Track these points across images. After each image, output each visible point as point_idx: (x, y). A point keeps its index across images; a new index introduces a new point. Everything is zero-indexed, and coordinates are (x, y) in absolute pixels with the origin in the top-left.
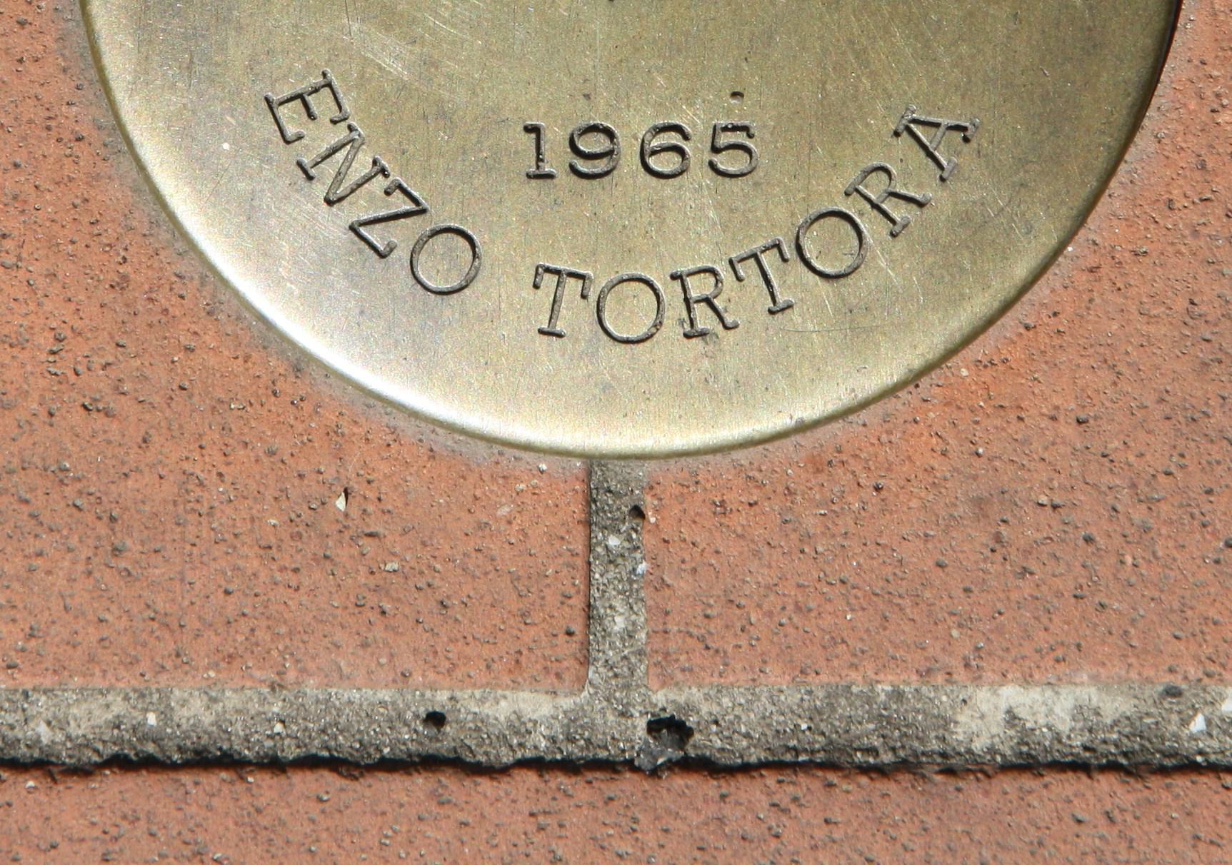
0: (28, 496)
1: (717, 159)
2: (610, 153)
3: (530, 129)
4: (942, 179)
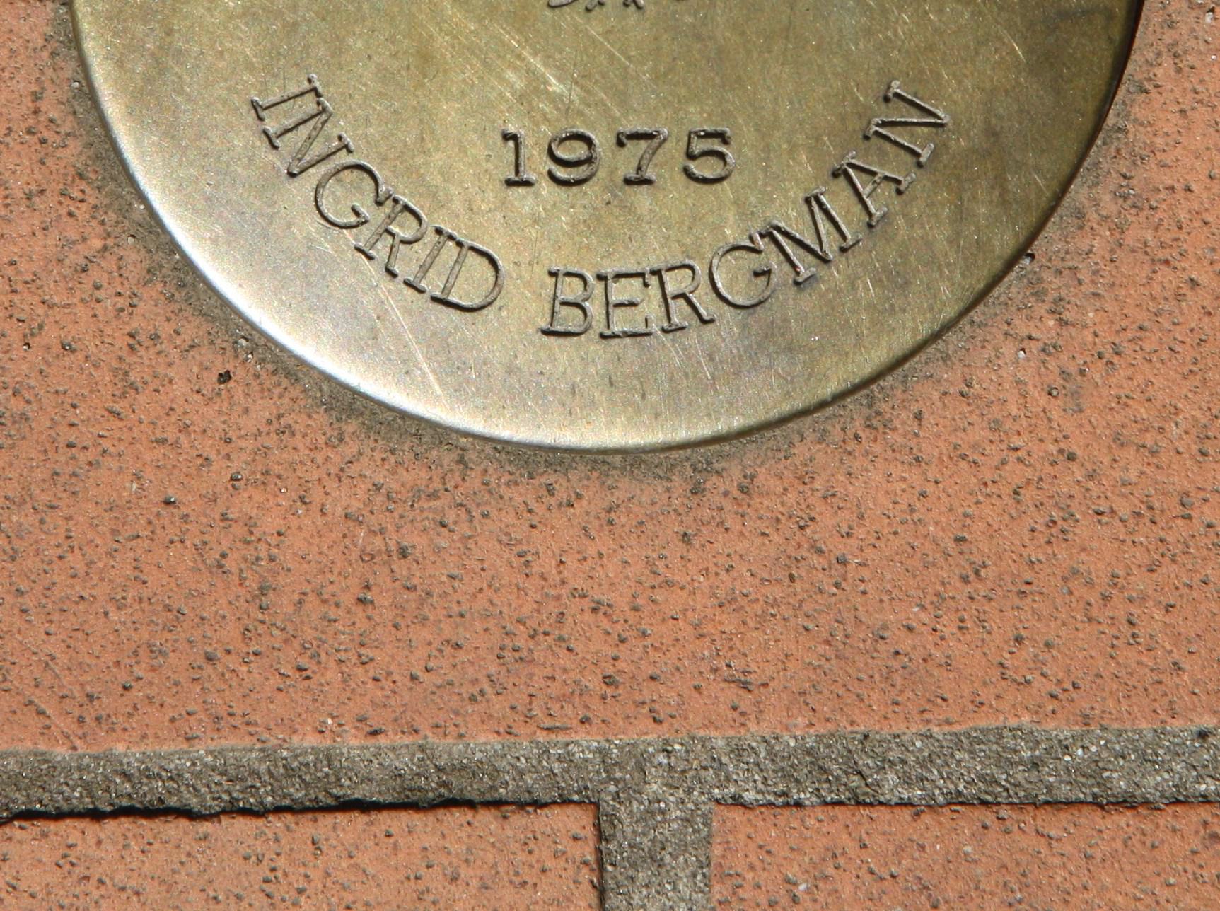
0: (836, 625)
1: (692, 166)
2: (589, 160)
4: (870, 226)
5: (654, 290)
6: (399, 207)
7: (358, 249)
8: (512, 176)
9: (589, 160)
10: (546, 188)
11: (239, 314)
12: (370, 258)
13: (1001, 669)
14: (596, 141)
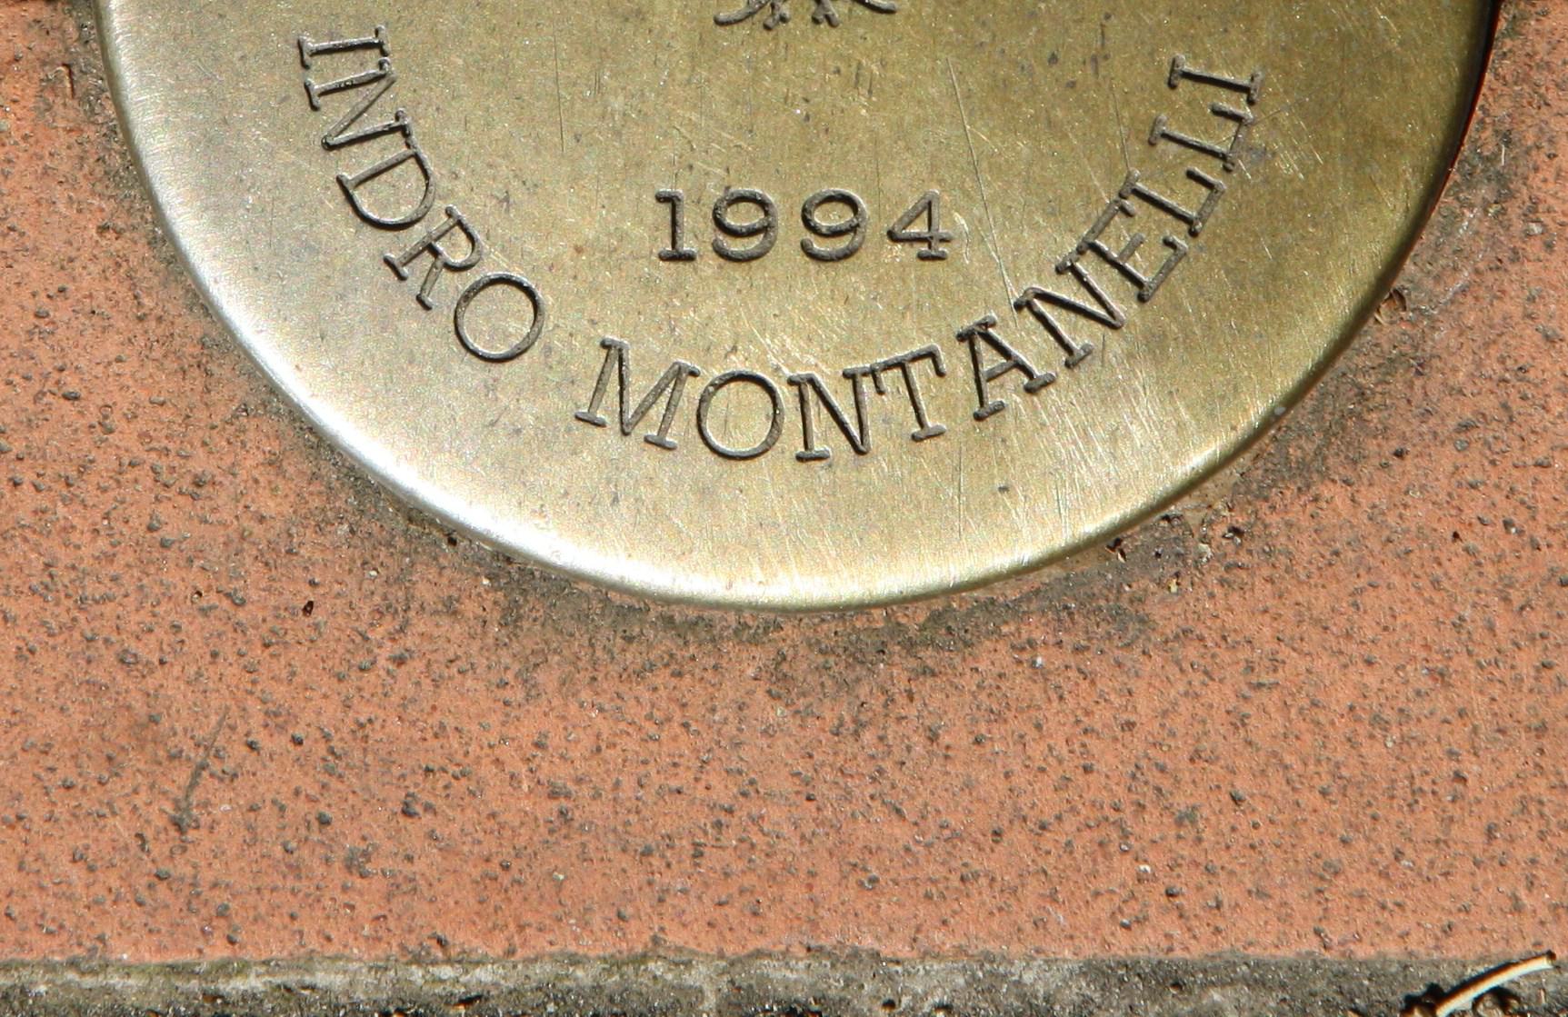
2: (764, 229)
3: (670, 200)
7: (388, 262)
9: (853, 229)
10: (709, 264)
11: (862, 608)
12: (402, 278)
14: (771, 198)
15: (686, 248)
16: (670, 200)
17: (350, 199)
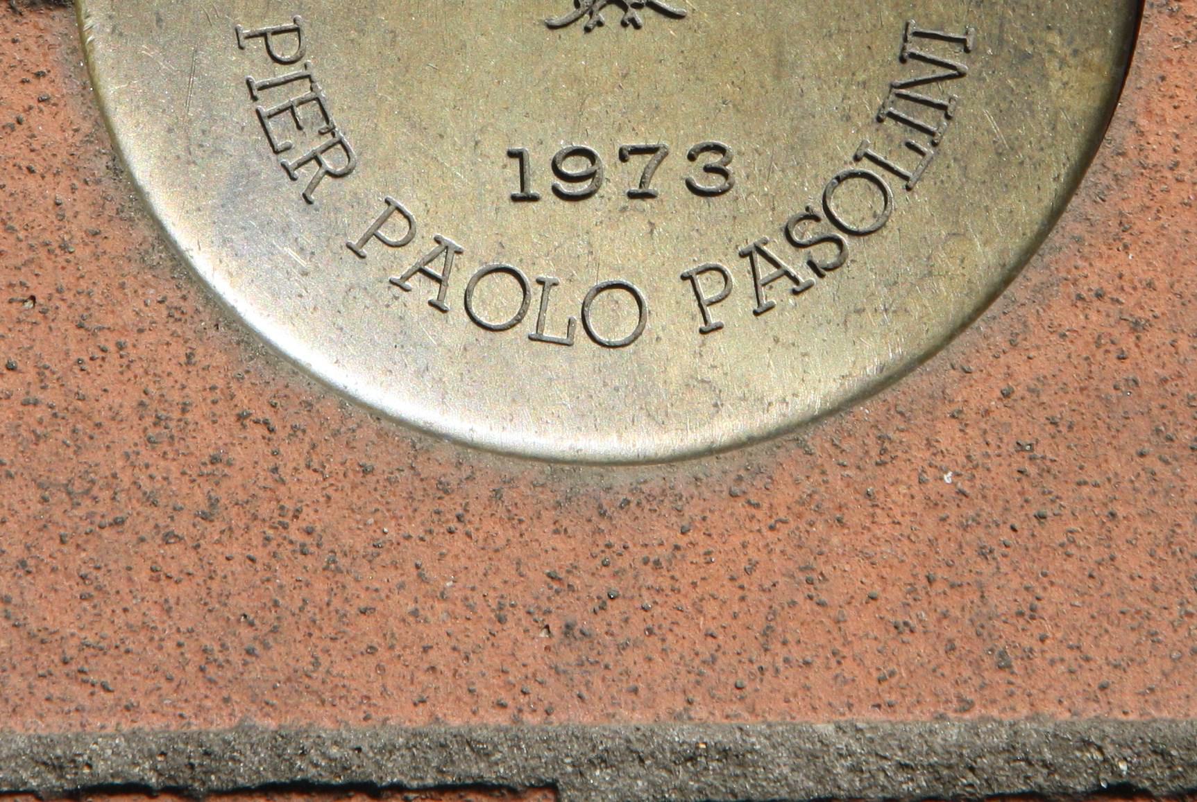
2: (591, 175)
3: (517, 155)
5: (319, 144)
6: (391, 208)
8: (517, 192)
12: (293, 179)
13: (672, 582)
15: (532, 191)
16: (517, 155)
17: (263, 125)
